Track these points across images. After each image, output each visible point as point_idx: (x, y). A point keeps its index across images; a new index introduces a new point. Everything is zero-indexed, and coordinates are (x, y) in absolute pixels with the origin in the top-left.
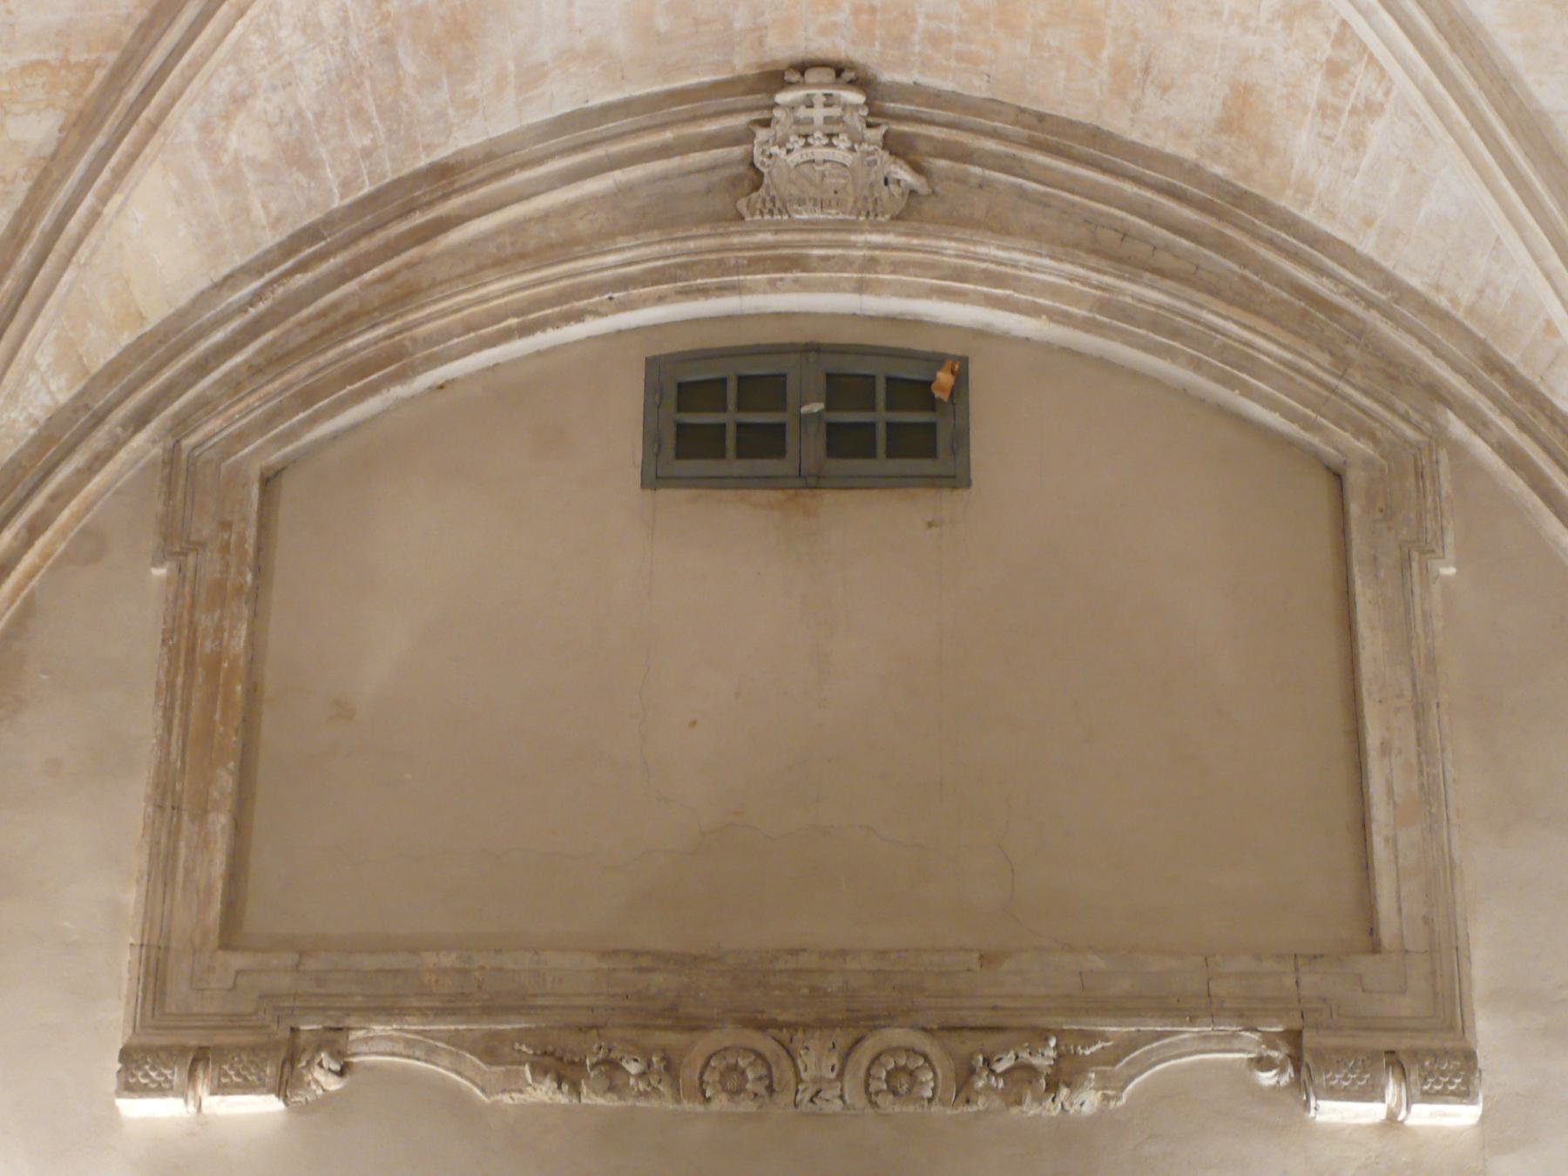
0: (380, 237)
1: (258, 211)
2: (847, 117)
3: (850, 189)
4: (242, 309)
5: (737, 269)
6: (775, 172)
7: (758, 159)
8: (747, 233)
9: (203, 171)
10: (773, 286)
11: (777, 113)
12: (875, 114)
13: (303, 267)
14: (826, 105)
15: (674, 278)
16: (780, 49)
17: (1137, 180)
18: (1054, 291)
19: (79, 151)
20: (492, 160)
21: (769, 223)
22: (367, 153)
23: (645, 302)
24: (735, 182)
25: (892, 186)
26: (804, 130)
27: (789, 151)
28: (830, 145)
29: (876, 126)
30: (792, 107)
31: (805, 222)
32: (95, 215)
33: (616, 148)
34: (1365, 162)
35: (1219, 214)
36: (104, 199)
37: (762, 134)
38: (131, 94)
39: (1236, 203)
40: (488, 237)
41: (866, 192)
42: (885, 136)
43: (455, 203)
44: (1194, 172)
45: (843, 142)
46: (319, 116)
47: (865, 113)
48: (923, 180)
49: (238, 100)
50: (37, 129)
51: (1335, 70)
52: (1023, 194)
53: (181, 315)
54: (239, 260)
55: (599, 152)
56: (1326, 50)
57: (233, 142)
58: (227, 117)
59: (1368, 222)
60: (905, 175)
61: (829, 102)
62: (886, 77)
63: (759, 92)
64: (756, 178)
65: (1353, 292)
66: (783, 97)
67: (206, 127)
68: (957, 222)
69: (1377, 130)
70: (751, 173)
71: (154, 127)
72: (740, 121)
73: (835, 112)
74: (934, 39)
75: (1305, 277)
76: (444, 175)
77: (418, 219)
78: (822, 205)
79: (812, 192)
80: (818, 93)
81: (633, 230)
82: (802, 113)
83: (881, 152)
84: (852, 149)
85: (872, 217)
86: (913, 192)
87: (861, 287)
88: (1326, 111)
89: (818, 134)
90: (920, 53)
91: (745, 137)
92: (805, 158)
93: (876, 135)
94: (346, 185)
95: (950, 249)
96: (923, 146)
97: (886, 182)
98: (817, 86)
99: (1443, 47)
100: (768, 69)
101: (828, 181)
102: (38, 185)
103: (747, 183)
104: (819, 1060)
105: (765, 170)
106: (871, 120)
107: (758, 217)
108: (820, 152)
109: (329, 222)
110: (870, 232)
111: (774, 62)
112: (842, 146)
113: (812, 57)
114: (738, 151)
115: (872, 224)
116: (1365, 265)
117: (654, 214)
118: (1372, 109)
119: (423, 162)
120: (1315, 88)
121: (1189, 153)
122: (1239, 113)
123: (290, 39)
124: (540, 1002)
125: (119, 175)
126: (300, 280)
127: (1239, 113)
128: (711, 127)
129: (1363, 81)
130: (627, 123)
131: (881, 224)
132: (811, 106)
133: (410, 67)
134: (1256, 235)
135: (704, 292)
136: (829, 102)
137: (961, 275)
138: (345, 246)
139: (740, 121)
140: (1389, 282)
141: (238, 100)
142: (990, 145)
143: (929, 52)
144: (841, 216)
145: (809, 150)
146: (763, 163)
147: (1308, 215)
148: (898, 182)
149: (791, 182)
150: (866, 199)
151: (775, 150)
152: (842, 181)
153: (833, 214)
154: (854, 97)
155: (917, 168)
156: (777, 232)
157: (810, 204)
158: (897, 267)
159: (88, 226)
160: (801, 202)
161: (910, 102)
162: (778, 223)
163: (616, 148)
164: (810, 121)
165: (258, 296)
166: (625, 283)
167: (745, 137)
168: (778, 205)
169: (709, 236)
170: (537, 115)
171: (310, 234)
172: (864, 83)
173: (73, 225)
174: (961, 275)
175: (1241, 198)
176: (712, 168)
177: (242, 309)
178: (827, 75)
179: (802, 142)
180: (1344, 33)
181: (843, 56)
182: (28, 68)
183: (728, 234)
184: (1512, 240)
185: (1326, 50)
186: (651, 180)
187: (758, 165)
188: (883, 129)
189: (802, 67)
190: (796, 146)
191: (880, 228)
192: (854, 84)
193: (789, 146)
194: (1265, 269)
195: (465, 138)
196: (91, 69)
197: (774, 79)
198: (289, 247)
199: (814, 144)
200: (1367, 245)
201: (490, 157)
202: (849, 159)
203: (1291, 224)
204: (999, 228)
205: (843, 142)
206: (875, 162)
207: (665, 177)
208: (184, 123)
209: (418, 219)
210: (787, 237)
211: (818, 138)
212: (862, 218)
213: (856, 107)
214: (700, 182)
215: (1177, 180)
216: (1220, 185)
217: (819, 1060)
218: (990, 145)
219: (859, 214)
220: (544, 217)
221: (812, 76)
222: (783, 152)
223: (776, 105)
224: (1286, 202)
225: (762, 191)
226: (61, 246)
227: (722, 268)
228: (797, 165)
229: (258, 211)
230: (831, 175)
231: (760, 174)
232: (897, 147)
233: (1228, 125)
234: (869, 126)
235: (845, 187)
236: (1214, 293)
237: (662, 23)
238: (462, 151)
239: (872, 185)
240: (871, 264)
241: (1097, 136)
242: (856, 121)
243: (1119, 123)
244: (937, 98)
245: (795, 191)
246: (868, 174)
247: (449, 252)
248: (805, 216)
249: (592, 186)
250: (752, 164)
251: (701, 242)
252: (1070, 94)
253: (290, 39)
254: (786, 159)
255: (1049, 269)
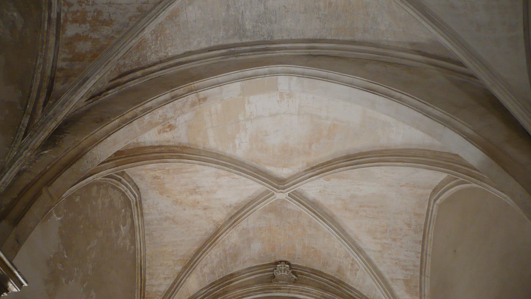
0: (223, 284)
1: (207, 280)
4: (203, 294)
5: (272, 290)
9: (200, 274)
10: (276, 292)
12: (290, 268)
13: (212, 288)
15: (263, 291)
16: (278, 259)
17: (326, 278)
18: (315, 294)
19: (184, 272)
20: (239, 273)
22: (222, 272)
23: (259, 294)
32: (185, 280)
33: (255, 272)
34: (357, 277)
35: (338, 284)
36: (187, 278)
37: (275, 271)
38: (192, 264)
39: (339, 282)
40: (237, 284)
43: (233, 279)
44: (334, 277)
45: (286, 272)
46: (216, 267)
49: (206, 265)
50: (179, 268)
51: (352, 265)
52: (311, 280)
53: (195, 294)
54: (203, 287)
55: (253, 273)
56: (351, 262)
57: (204, 270)
58: (204, 267)
59: (358, 286)
60: (294, 277)
61: (284, 266)
62: (292, 263)
64: (274, 277)
65: (356, 295)
67: (201, 268)
68: (302, 284)
69: (358, 272)
71: (194, 268)
72: (272, 269)
74: (298, 258)
75: (350, 293)
76: (232, 275)
77: (228, 281)
78: (283, 281)
81: (257, 284)
87: (288, 293)
88: (351, 270)
91: (273, 271)
94: (219, 276)
95: (301, 287)
98: (283, 264)
99: (366, 262)
102: (178, 276)
108: (283, 274)
109: (216, 281)
114: (272, 273)
116: (358, 292)
117: (260, 281)
118: (358, 270)
119: (229, 274)
120: (350, 267)
121: (333, 275)
122: (340, 270)
123: (213, 257)
124: (423, 278)
125: (189, 275)
126: (212, 290)
127: (340, 270)
129: (356, 266)
130: (257, 269)
133: (229, 261)
134: (342, 287)
135: (267, 293)
136: (284, 266)
137: (302, 291)
138: (218, 285)
139: (272, 269)
140: (361, 294)
141: (206, 265)
142: (306, 273)
147: (350, 284)
153: (285, 282)
154: (288, 266)
155: (296, 276)
158: (294, 290)
159: (184, 282)
163: (255, 272)
165: (206, 292)
166: (256, 291)
167: (273, 271)
168: (277, 281)
170: (245, 267)
171: (213, 283)
172: (289, 264)
173: (182, 282)
174: (302, 291)
175: (340, 281)
177: (203, 294)
178: (284, 263)
180: (353, 260)
182: (178, 260)
184: (378, 289)
185: (351, 262)
186: (260, 277)
189: (281, 262)
191: (291, 284)
192: (288, 264)
194: (344, 292)
195: (235, 270)
196: (187, 260)
197: (277, 263)
198: (210, 285)
199: (282, 272)
200: (358, 289)
201: (238, 273)
203: (347, 285)
204: (308, 285)
205: (286, 272)
207: (262, 276)
208: (198, 268)
209: (228, 281)
211: (283, 271)
215: (332, 279)
216: (337, 279)
218: (306, 273)
220: (245, 281)
221: (282, 263)
224: (346, 282)
226: (180, 285)
227: (269, 289)
229: (207, 280)
232: (294, 273)
233: (338, 271)
236: (338, 295)
237: (262, 255)
238: (129, 145)
240: (290, 289)
241: (321, 272)
242: (288, 269)
243: (323, 270)
244: (299, 266)
247: (232, 286)
249: (252, 277)
251: (266, 286)
252: (317, 266)
253: (213, 257)
254: (278, 274)
255: (315, 291)
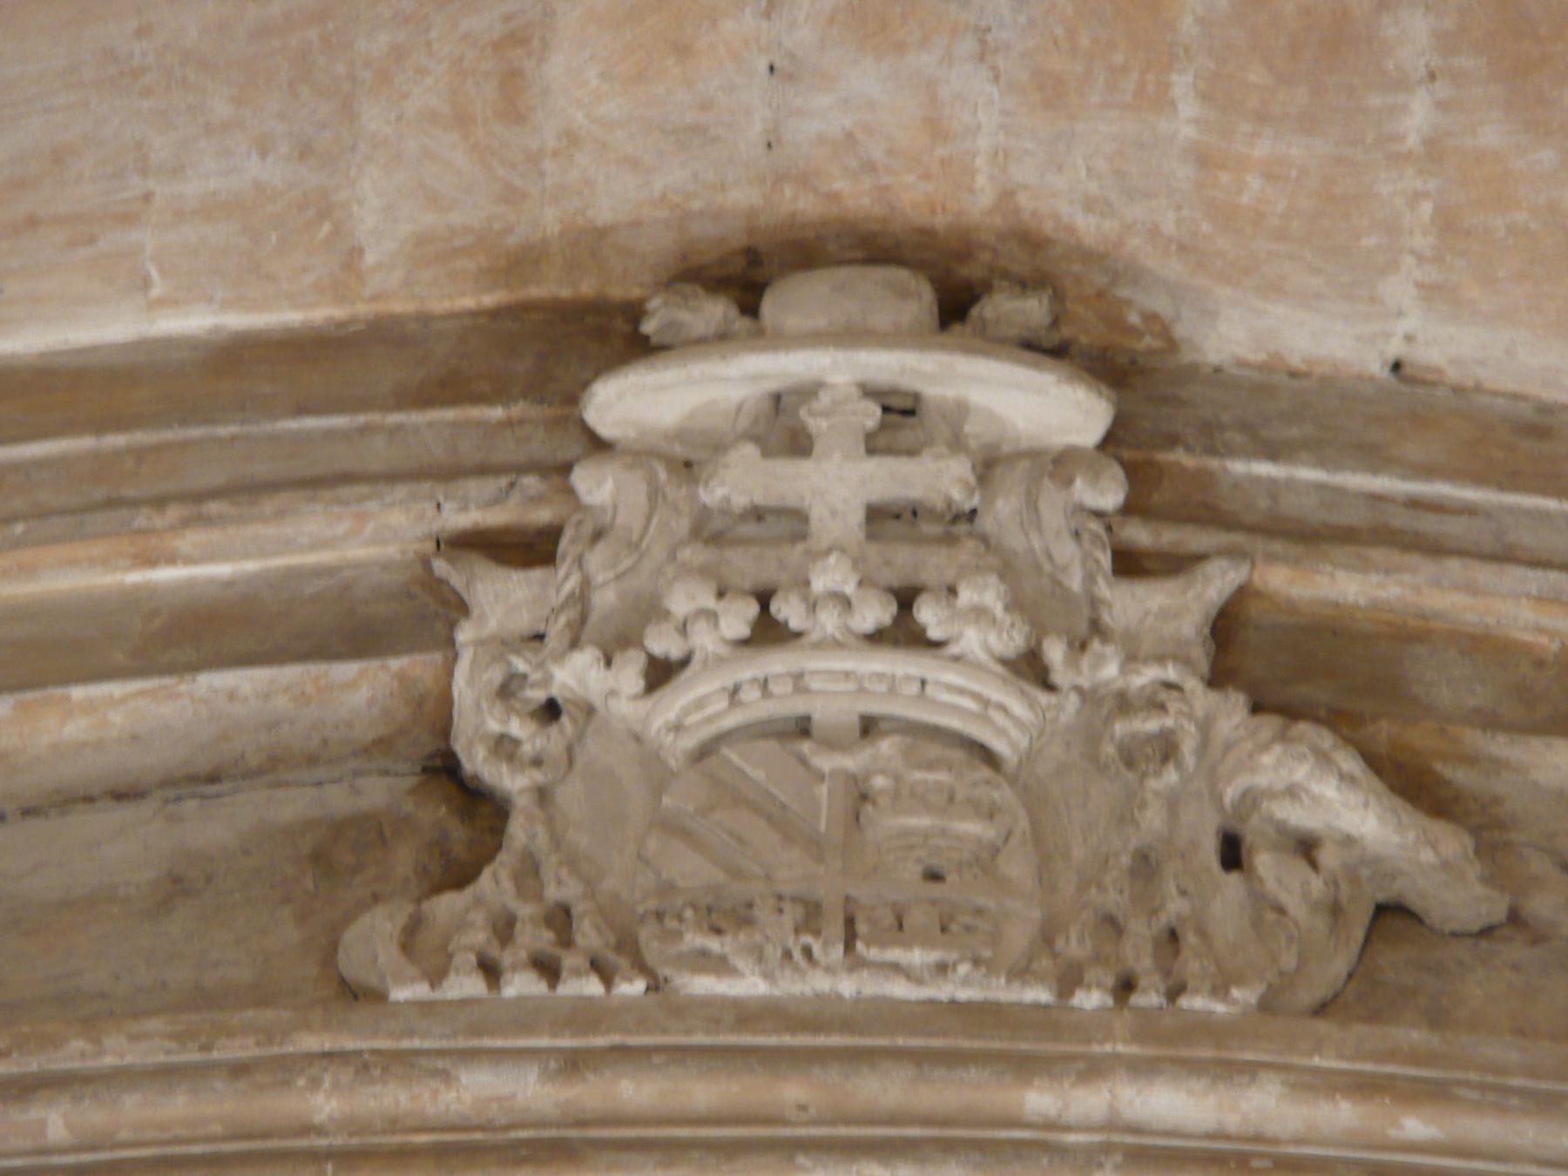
2: (1003, 511)
3: (1017, 866)
6: (571, 795)
7: (481, 726)
8: (398, 1063)
11: (596, 485)
14: (874, 445)
21: (526, 1017)
24: (335, 857)
25: (1264, 862)
26: (745, 565)
27: (660, 673)
28: (902, 632)
29: (1176, 564)
30: (684, 458)
31: (747, 1014)
37: (502, 599)
41: (1113, 898)
42: (1226, 627)
45: (976, 623)
47: (1109, 494)
48: (1452, 842)
60: (1342, 805)
62: (1231, 332)
63: (498, 394)
66: (625, 402)
70: (436, 813)
73: (938, 478)
79: (791, 869)
80: (839, 369)
82: (742, 480)
83: (1201, 698)
84: (1030, 668)
85: (1149, 998)
86: (1392, 915)
89: (831, 576)
90: (1434, 151)
91: (418, 613)
92: (756, 708)
93: (1176, 608)
96: (1446, 685)
97: (1232, 853)
100: (549, 287)
101: (887, 823)
103: (404, 859)
104: (1032, 503)
105: (512, 782)
106: (1139, 535)
107: (466, 985)
108: (838, 675)
110: (1143, 1069)
111: (590, 242)
112: (972, 640)
113: (804, 205)
114: (360, 689)
115: (1146, 1028)
128: (206, 563)
131: (1205, 1027)
132: (799, 444)
139: (363, 539)
143: (1491, 135)
144: (963, 988)
145: (777, 662)
146: (504, 747)
148: (1306, 847)
149: (671, 827)
150: (1112, 925)
151: (574, 673)
152: (971, 827)
153: (906, 976)
155: (1411, 782)
156: (573, 1064)
157: (779, 929)
160: (727, 915)
161: (1373, 457)
162: (585, 1016)
164: (792, 523)
167: (418, 613)
169: (166, 1075)
176: (205, 779)
179: (738, 618)
181: (977, 202)
183: (285, 1068)
187: (477, 762)
188: (1216, 583)
190: (705, 640)
193: (663, 643)
202: (1011, 719)
205: (976, 623)
206: (1167, 748)
210: (633, 1091)
211: (836, 590)
212: (1090, 999)
213: (1061, 464)
214: (126, 847)
217: (1032, 503)
219: (1069, 980)
221: (794, 301)
222: (629, 675)
223: (598, 445)
225: (495, 884)
228: (704, 752)
230: (901, 796)
231: (481, 807)
234: (1129, 564)
235: (986, 860)
239: (1145, 866)
242: (1058, 533)
245: (690, 870)
246: (1125, 817)
248: (750, 985)
250: (445, 769)
254: (625, 702)
